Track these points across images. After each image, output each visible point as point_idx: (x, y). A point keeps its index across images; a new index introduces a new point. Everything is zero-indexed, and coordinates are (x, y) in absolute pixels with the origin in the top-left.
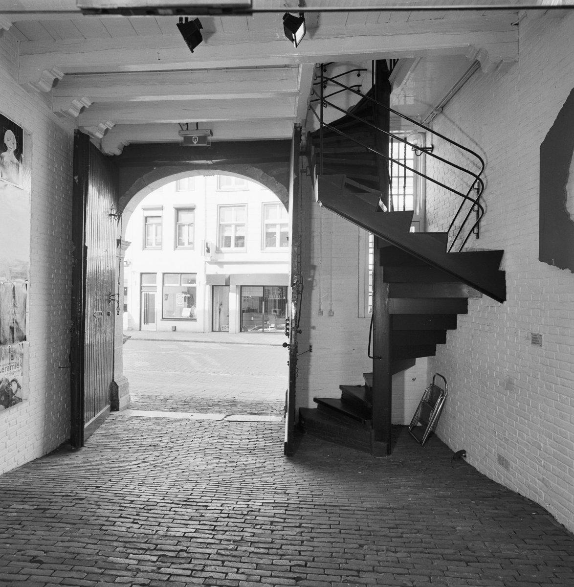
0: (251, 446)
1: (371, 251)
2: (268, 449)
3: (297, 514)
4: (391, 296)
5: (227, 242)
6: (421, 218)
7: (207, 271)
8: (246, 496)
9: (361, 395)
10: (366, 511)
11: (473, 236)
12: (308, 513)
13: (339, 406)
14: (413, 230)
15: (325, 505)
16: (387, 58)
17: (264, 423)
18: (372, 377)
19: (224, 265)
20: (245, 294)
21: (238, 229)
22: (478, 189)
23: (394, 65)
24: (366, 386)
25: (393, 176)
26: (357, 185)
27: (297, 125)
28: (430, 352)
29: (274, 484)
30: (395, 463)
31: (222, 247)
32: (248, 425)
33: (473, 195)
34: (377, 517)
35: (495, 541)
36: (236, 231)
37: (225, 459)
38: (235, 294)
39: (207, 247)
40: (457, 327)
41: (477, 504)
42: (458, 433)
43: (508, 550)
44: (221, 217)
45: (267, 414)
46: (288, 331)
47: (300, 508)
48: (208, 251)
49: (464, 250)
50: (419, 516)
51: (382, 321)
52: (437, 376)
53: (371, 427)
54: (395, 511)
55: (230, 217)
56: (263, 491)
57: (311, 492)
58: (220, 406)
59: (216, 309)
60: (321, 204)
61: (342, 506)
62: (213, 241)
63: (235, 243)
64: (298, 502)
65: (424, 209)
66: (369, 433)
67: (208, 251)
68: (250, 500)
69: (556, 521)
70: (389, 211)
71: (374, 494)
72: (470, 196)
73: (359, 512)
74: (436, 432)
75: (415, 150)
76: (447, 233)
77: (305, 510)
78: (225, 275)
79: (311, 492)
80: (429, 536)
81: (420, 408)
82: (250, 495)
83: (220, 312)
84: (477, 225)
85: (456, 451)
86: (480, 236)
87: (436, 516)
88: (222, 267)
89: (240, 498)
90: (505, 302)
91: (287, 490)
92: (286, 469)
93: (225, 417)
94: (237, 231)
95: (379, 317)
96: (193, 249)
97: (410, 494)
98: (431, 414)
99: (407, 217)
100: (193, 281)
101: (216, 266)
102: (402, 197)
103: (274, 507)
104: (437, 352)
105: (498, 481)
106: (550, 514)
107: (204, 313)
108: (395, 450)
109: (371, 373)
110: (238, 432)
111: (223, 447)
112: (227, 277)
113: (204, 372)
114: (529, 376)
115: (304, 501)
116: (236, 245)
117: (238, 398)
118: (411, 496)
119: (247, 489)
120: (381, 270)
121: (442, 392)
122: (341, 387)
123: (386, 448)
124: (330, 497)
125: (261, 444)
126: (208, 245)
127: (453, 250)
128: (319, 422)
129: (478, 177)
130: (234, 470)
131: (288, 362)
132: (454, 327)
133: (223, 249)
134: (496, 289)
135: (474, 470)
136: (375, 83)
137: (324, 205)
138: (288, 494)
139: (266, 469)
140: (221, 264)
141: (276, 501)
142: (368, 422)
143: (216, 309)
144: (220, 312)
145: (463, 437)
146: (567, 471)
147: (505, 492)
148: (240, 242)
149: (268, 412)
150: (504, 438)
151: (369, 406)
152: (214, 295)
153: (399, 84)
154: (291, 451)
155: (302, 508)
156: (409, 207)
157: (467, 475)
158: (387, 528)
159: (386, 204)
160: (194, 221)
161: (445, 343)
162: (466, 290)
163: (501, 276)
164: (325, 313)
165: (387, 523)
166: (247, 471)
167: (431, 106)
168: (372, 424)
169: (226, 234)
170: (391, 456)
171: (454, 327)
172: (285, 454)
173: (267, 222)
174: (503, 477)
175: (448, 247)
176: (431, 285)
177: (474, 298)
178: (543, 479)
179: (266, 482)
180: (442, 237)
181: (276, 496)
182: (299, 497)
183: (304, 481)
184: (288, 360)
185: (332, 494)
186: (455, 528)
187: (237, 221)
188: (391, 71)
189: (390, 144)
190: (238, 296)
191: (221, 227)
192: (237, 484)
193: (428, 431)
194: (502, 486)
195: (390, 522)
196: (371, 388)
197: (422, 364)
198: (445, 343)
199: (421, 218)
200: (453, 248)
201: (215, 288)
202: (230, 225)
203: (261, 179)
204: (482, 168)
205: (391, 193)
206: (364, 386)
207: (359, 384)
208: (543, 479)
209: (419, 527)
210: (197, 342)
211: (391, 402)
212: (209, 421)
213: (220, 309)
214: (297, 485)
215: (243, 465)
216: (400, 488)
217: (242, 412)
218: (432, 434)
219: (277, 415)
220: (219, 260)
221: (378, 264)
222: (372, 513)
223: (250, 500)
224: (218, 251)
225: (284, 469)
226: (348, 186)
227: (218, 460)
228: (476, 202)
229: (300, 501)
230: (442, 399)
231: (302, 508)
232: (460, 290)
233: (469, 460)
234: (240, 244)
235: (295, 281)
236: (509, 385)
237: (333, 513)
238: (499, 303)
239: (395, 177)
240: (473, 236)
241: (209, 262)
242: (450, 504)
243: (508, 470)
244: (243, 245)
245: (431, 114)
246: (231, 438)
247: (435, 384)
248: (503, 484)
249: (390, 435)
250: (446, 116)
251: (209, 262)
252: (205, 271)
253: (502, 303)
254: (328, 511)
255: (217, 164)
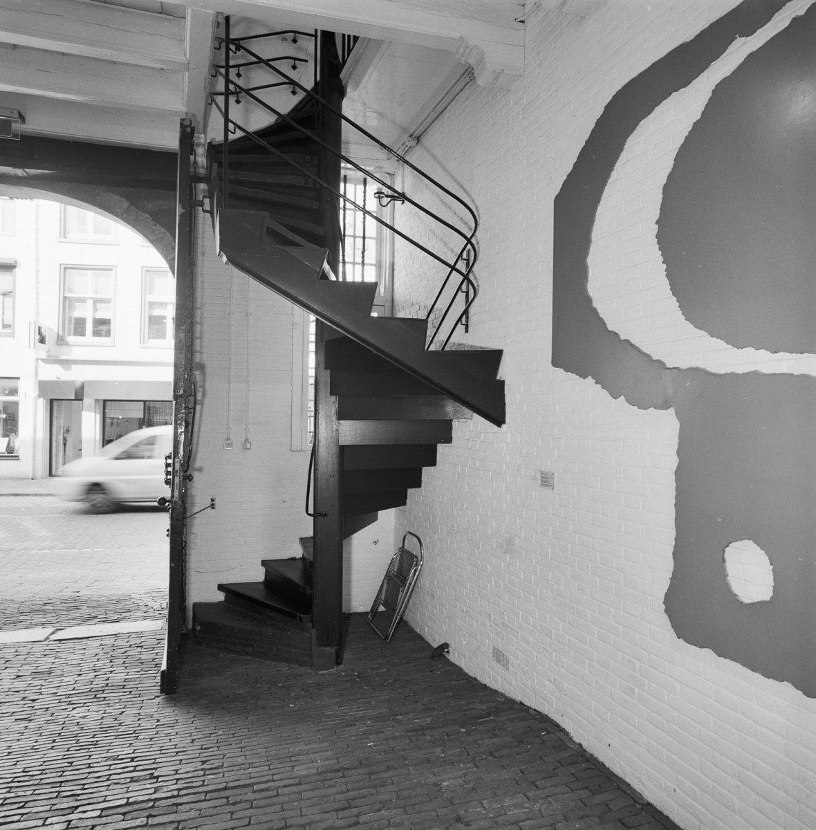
0: (99, 683)
1: (312, 347)
2: (132, 684)
3: (171, 819)
4: (342, 415)
5: (79, 327)
6: (387, 301)
7: (39, 375)
8: (70, 799)
9: (295, 575)
10: (300, 783)
11: (460, 328)
12: (193, 814)
13: (259, 595)
14: (374, 314)
15: (225, 789)
16: (338, 30)
17: (129, 635)
18: (312, 544)
19: (73, 366)
20: (111, 414)
21: (98, 307)
22: (468, 260)
23: (350, 51)
24: (303, 559)
25: (346, 233)
26: (290, 235)
27: (187, 123)
28: (398, 500)
29: (132, 760)
30: (347, 679)
31: (69, 334)
32: (97, 643)
33: (461, 266)
34: (317, 792)
35: (497, 795)
36: (95, 310)
37: (40, 720)
38: (93, 414)
39: (40, 333)
40: (437, 463)
41: (468, 733)
42: (440, 616)
43: (515, 808)
44: (67, 286)
45: (136, 619)
46: (169, 477)
47: (177, 805)
48: (42, 341)
49: (447, 349)
50: (385, 775)
51: (327, 456)
52: (409, 536)
53: (310, 625)
54: (347, 773)
55: (83, 285)
56: (108, 780)
57: (203, 762)
58: (44, 612)
59: (58, 439)
60: (225, 259)
61: (256, 784)
62: (52, 325)
63: (93, 331)
64: (175, 793)
65: (391, 289)
66: (308, 635)
67: (42, 341)
68: (77, 807)
69: (571, 739)
70: (341, 279)
71: (313, 746)
72: (457, 267)
73: (286, 790)
74: (405, 618)
75: (379, 198)
76: (426, 321)
77: (188, 807)
78: (73, 382)
79: (203, 762)
80: (401, 810)
81: (385, 585)
82: (79, 795)
83: (65, 444)
84: (466, 312)
85: (435, 645)
86: (470, 329)
87: (410, 768)
88: (69, 369)
89: (54, 808)
90: (503, 426)
91: (156, 769)
92: (163, 721)
93: (53, 633)
94: (97, 310)
95: (323, 452)
96: (12, 335)
97: (369, 734)
98: (400, 593)
99: (366, 292)
100: (14, 392)
101: (57, 367)
102: (360, 266)
103: (124, 814)
104: (408, 500)
105: (493, 685)
106: (563, 730)
107: (34, 447)
108: (347, 656)
109: (312, 537)
110: (74, 659)
111: (41, 693)
112: (78, 385)
113: (25, 549)
114: (536, 532)
115: (187, 788)
116: (96, 333)
117: (85, 593)
118: (372, 737)
119: (74, 783)
120: (326, 376)
121: (415, 559)
122: (264, 563)
123: (334, 656)
124: (235, 768)
125: (118, 677)
126: (43, 330)
127: (432, 348)
128: (227, 626)
129: (469, 241)
130: (54, 741)
131: (168, 531)
132: (433, 462)
133: (71, 339)
134: (493, 409)
135: (459, 672)
136: (318, 79)
137: (231, 261)
138: (158, 777)
139: (122, 728)
140: (66, 363)
141: (131, 800)
142: (306, 617)
143: (58, 439)
144: (65, 444)
145: (445, 625)
146: (587, 667)
147: (503, 703)
148: (104, 328)
149: (139, 614)
150: (502, 623)
151: (308, 592)
152: (55, 415)
153: (357, 86)
154: (170, 686)
155: (181, 804)
156: (370, 278)
157: (452, 682)
158: (332, 811)
159: (336, 272)
160: (14, 287)
161: (419, 486)
162: (450, 407)
163: (499, 388)
164: (237, 443)
165: (334, 801)
166: (82, 739)
167: (405, 130)
168: (312, 621)
169: (78, 313)
170: (342, 667)
171: (433, 462)
172: (162, 691)
173: (150, 298)
174: (500, 679)
175: (428, 340)
176: (405, 393)
177: (461, 420)
178: (555, 679)
179: (116, 758)
180: (418, 326)
181: (135, 786)
182: (177, 780)
183: (193, 741)
184: (169, 527)
185: (241, 760)
186: (438, 785)
187: (96, 293)
188: (344, 62)
189: (342, 185)
190: (99, 417)
191: (67, 303)
192: (54, 775)
193: (396, 619)
194: (498, 692)
195: (337, 797)
196: (311, 562)
197: (387, 518)
198: (419, 486)
199: (387, 301)
200: (432, 345)
201: (55, 403)
202: (83, 300)
203: (125, 216)
204: (473, 229)
205: (344, 259)
206: (301, 559)
207: (292, 556)
208: (555, 679)
209: (386, 797)
210: (18, 495)
211: (341, 566)
212: (18, 645)
213: (65, 439)
214: (177, 753)
215: (76, 728)
216: (355, 725)
217: (87, 619)
218: (402, 623)
219: (153, 618)
220: (63, 357)
221: (322, 366)
222: (308, 787)
223: (77, 807)
224: (61, 340)
225: (158, 721)
226: (272, 233)
227: (24, 723)
228: (466, 277)
229: (179, 790)
230: (415, 571)
231: (181, 804)
232: (443, 407)
233: (453, 657)
234: (103, 333)
235: (181, 392)
236: (509, 546)
237: (240, 802)
238: (496, 427)
239: (350, 263)
240: (460, 328)
241: (42, 360)
242: (431, 741)
243: (507, 669)
244: (108, 334)
245: (403, 145)
246: (59, 673)
247: (406, 548)
248: (500, 690)
249: (339, 628)
250: (425, 149)
251: (42, 360)
252: (36, 375)
253: (500, 427)
254: (231, 800)
255: (36, 177)
